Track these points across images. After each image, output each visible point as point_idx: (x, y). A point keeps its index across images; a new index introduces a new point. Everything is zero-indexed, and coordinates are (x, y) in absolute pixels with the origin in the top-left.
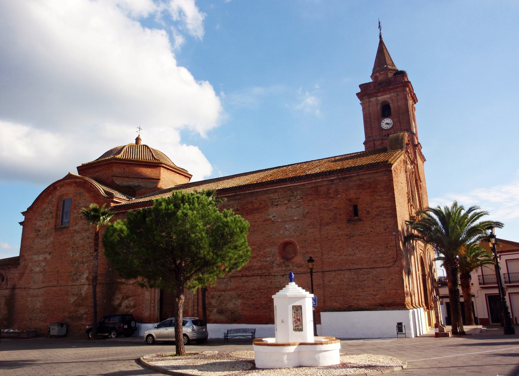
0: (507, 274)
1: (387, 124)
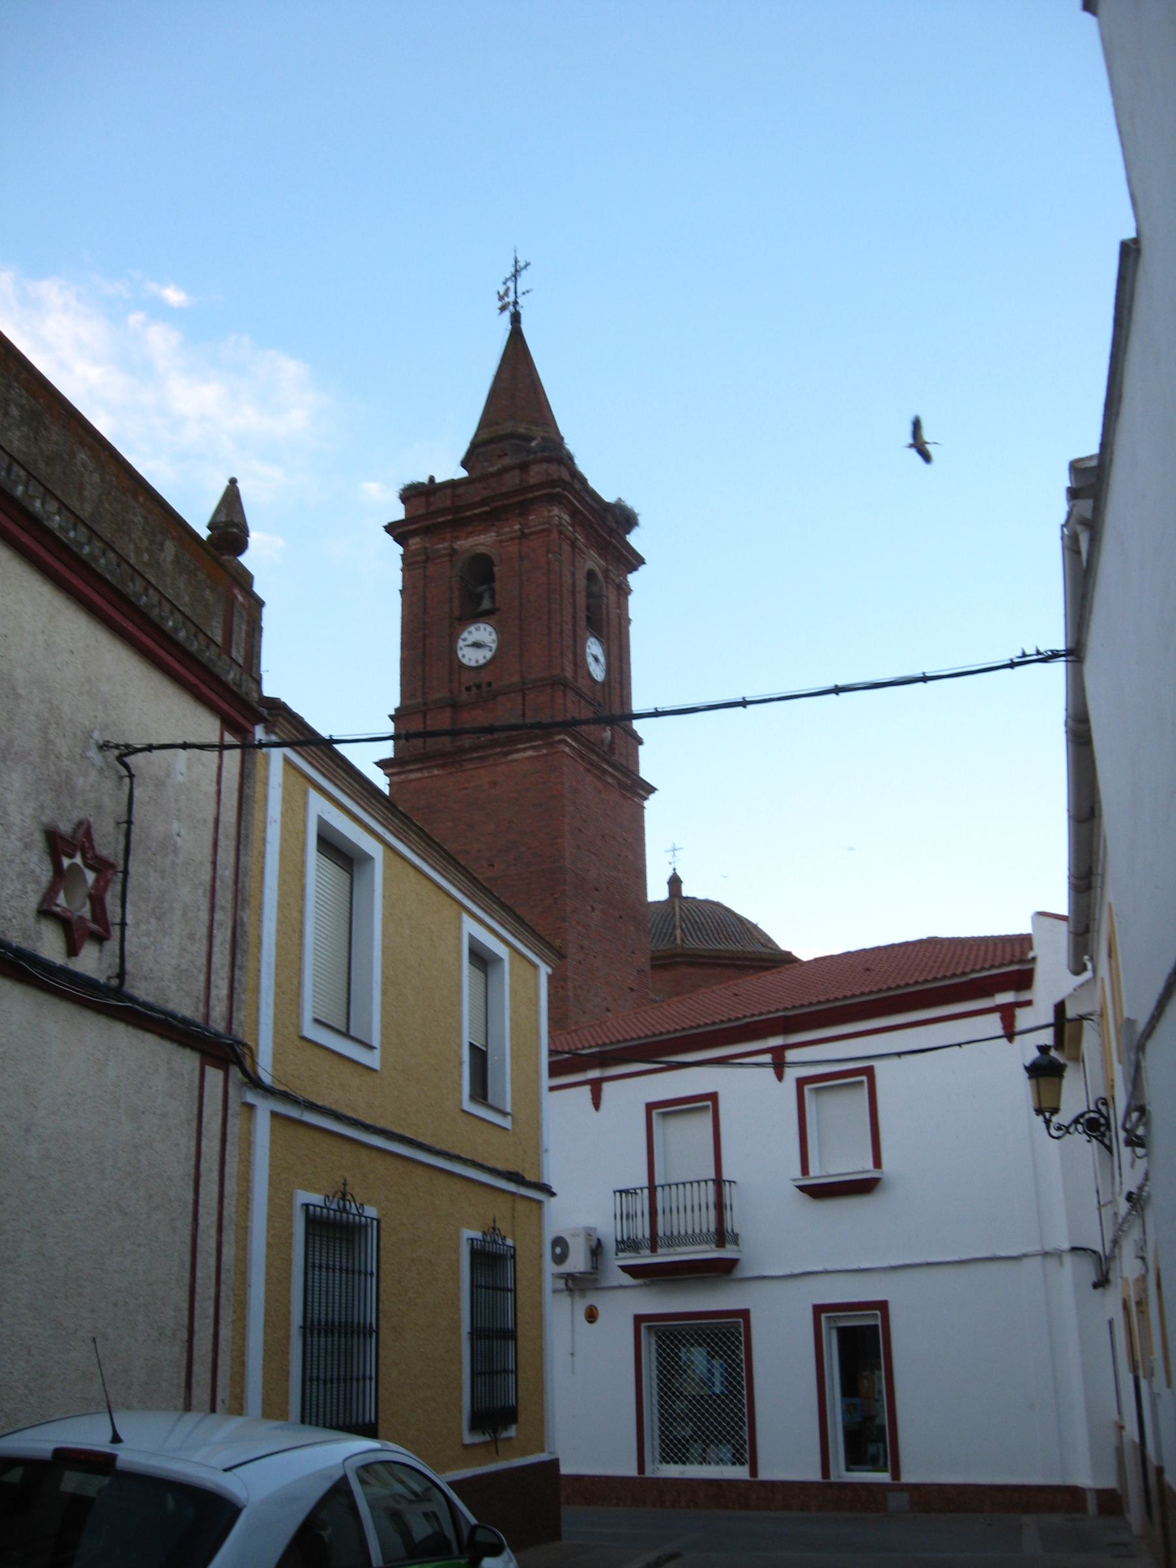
0: (646, 1192)
1: (477, 645)
